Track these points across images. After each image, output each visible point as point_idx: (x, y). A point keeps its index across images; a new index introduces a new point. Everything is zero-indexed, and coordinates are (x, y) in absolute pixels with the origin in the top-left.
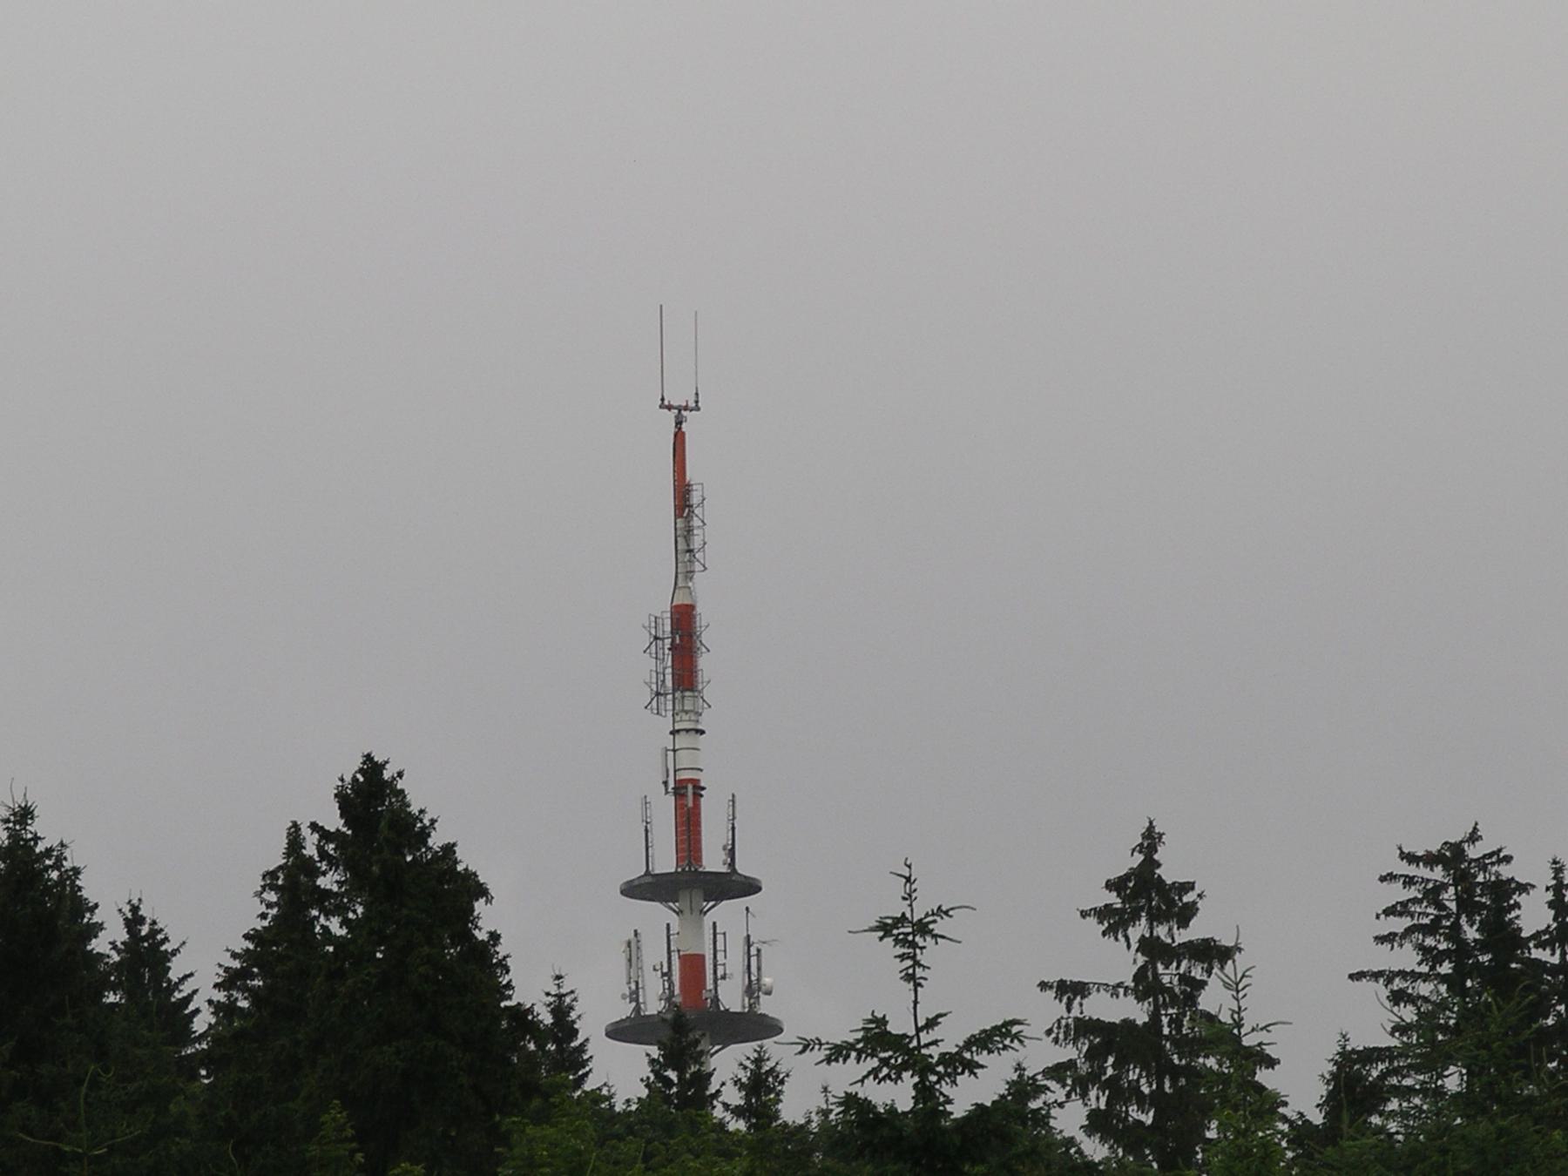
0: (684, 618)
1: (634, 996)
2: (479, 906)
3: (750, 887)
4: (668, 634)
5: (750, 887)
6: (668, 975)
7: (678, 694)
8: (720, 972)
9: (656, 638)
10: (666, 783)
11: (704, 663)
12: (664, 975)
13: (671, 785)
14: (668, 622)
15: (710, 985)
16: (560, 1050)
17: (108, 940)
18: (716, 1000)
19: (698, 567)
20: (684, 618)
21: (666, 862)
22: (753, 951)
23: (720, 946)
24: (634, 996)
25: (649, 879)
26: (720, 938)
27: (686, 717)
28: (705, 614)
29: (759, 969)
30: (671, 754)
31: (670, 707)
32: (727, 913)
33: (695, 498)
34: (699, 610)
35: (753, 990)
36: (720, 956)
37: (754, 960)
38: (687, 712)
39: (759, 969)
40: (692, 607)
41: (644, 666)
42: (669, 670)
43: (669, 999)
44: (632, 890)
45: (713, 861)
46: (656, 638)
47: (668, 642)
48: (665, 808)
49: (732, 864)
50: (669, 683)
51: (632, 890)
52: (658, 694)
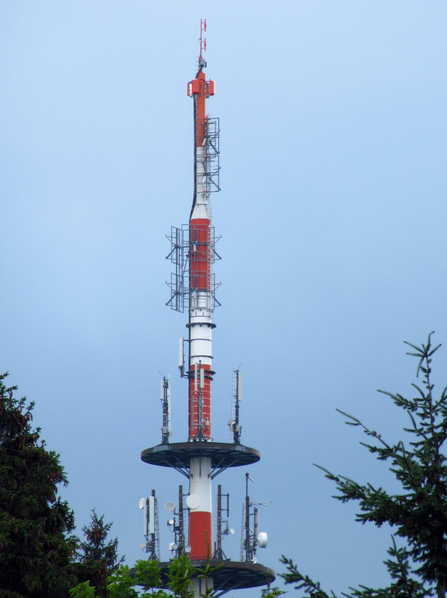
0: (200, 231)
1: (151, 547)
2: (59, 485)
3: (250, 457)
4: (186, 244)
5: (250, 457)
6: (178, 529)
7: (194, 294)
8: (223, 528)
9: (177, 247)
10: (182, 368)
11: (216, 269)
12: (176, 529)
13: (186, 369)
14: (187, 233)
15: (214, 539)
16: (364, 506)
17: (79, 533)
18: (219, 552)
19: (213, 188)
20: (200, 231)
21: (180, 435)
22: (251, 511)
23: (224, 506)
24: (151, 547)
25: (166, 448)
26: (224, 500)
27: (199, 313)
28: (217, 229)
29: (256, 526)
30: (187, 343)
31: (187, 304)
32: (232, 475)
33: (211, 129)
34: (212, 224)
35: (250, 545)
36: (224, 513)
37: (251, 518)
38: (201, 309)
39: (256, 526)
40: (207, 221)
41: (164, 270)
42: (187, 274)
43: (180, 549)
44: (150, 457)
45: (220, 435)
46: (177, 247)
47: (186, 250)
48: (179, 390)
49: (237, 435)
50: (187, 284)
51: (150, 457)
52: (177, 293)
